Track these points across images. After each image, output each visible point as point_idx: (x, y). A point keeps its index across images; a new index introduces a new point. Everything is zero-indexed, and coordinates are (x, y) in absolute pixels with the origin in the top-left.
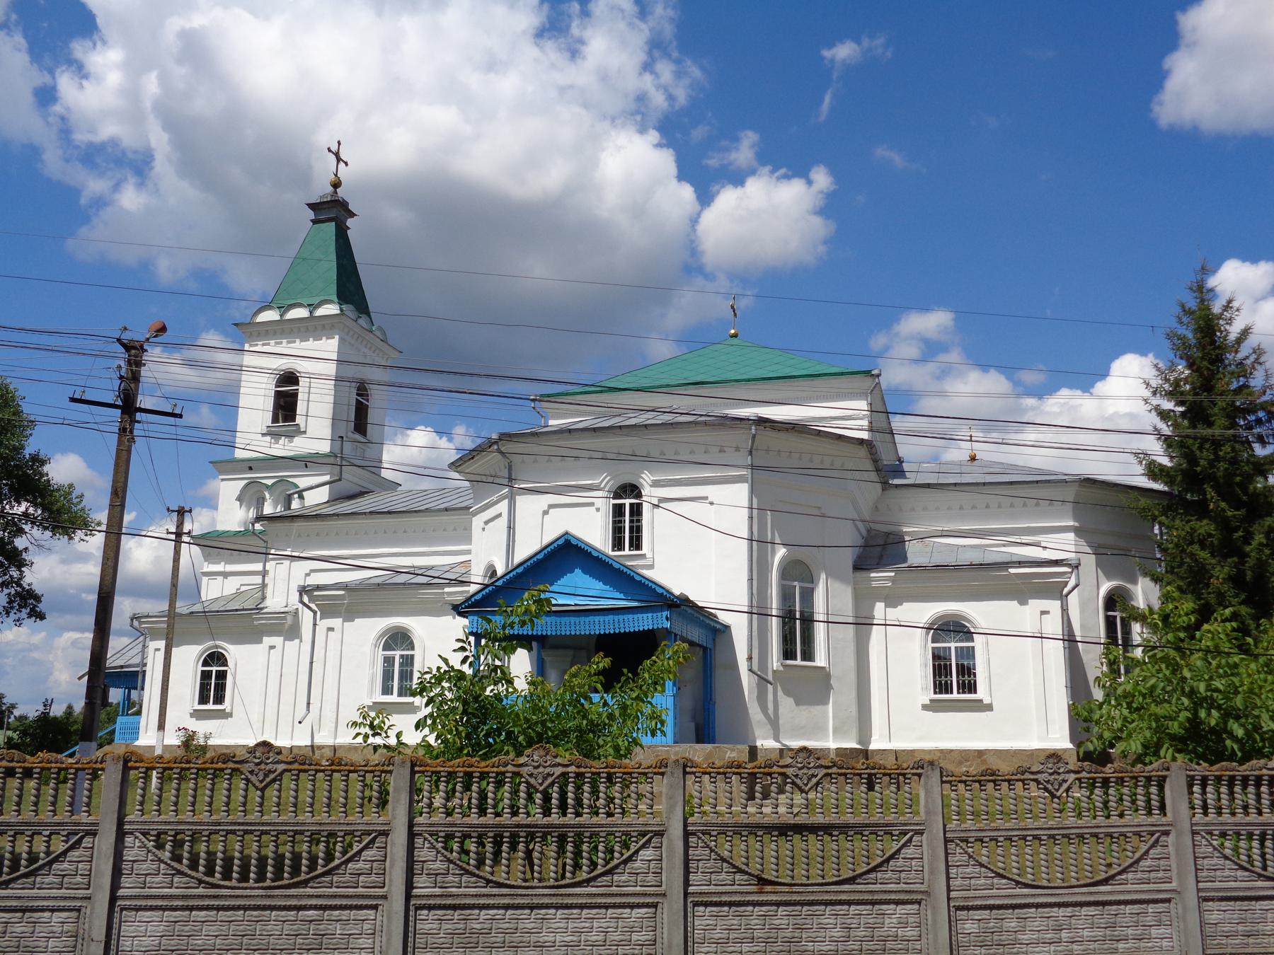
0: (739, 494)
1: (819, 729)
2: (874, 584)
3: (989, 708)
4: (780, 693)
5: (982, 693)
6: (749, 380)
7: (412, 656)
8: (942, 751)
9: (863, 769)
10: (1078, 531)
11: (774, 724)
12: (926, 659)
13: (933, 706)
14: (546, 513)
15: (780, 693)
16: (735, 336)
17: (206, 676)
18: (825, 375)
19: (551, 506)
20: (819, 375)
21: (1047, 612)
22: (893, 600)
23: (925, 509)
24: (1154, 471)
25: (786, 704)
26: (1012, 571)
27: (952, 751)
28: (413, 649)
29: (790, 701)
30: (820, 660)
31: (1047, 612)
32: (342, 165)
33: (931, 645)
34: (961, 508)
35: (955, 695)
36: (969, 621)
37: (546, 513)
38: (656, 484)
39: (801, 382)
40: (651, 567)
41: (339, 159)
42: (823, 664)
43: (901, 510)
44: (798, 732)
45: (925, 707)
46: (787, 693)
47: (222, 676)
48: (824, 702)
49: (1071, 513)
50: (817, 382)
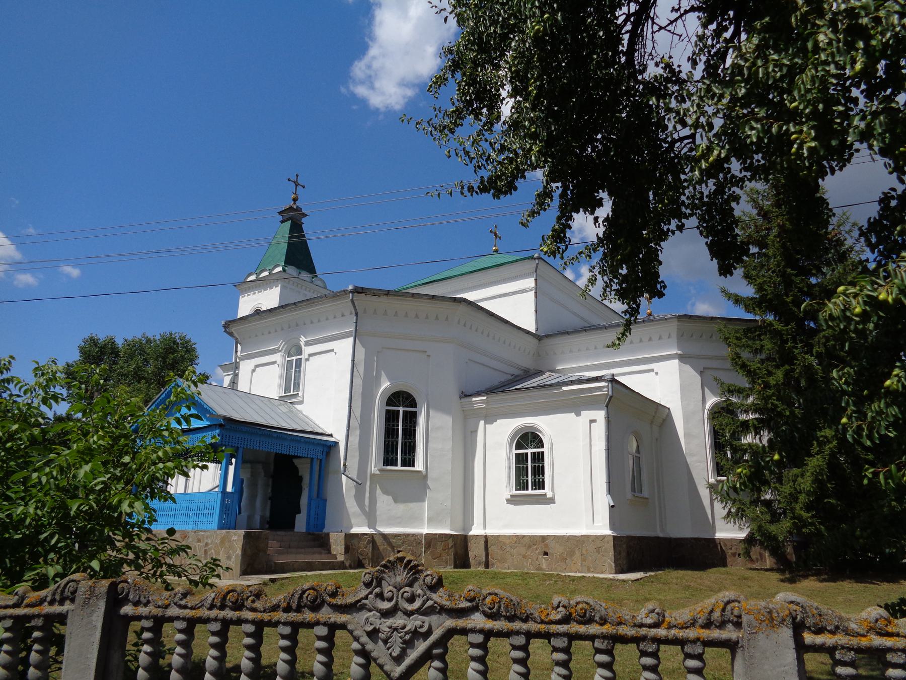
0: (344, 347)
1: (415, 519)
2: (476, 406)
3: (552, 501)
4: (379, 491)
5: (547, 491)
6: (462, 275)
7: (543, 453)
8: (517, 536)
9: (459, 549)
10: (682, 358)
11: (371, 518)
12: (510, 463)
13: (514, 500)
14: (254, 371)
15: (379, 491)
16: (496, 251)
17: (521, 459)
18: (506, 263)
19: (257, 366)
20: (502, 264)
21: (594, 421)
22: (490, 419)
23: (571, 351)
24: (749, 304)
25: (384, 502)
26: (565, 388)
27: (524, 536)
28: (542, 446)
29: (388, 499)
30: (419, 466)
31: (594, 421)
32: (299, 188)
33: (515, 452)
34: (596, 348)
35: (530, 491)
36: (540, 432)
37: (254, 371)
38: (308, 344)
39: (490, 271)
40: (301, 402)
41: (297, 184)
42: (420, 469)
43: (555, 354)
44: (391, 522)
45: (509, 501)
46: (386, 492)
47: (539, 458)
48: (421, 499)
49: (676, 344)
50: (502, 269)
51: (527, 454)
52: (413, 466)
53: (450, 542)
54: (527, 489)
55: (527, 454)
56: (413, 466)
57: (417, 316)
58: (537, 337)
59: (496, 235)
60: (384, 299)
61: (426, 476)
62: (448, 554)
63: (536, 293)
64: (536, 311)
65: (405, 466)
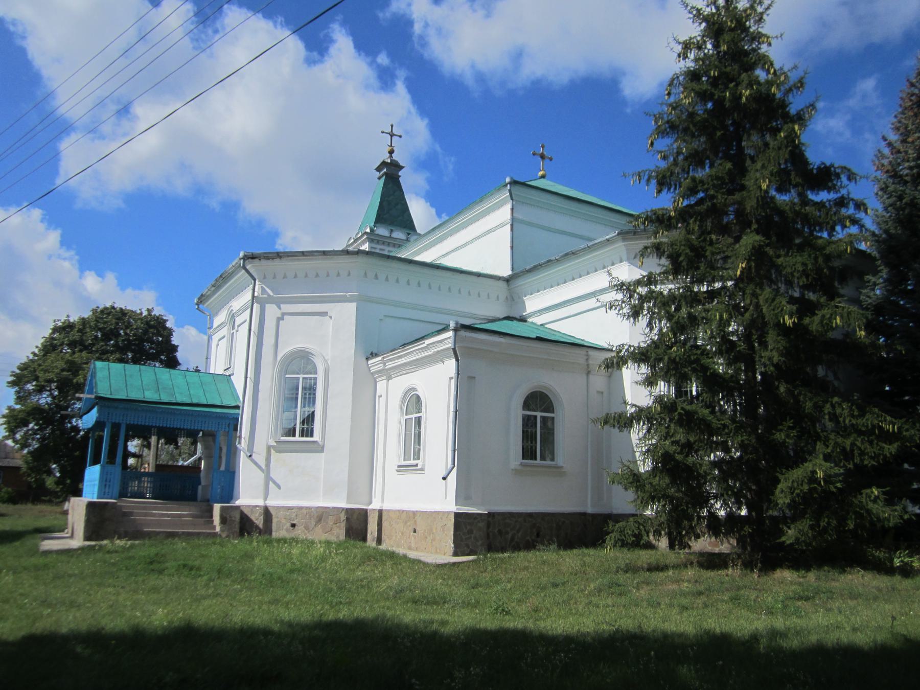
0: (350, 309)
17: (528, 422)
30: (317, 437)
32: (394, 138)
41: (392, 135)
51: (535, 417)
52: (312, 436)
53: (343, 516)
54: (536, 459)
55: (535, 417)
56: (312, 436)
57: (317, 275)
58: (508, 280)
59: (542, 157)
60: (277, 262)
61: (323, 446)
62: (339, 527)
63: (512, 225)
64: (512, 247)
65: (302, 436)
